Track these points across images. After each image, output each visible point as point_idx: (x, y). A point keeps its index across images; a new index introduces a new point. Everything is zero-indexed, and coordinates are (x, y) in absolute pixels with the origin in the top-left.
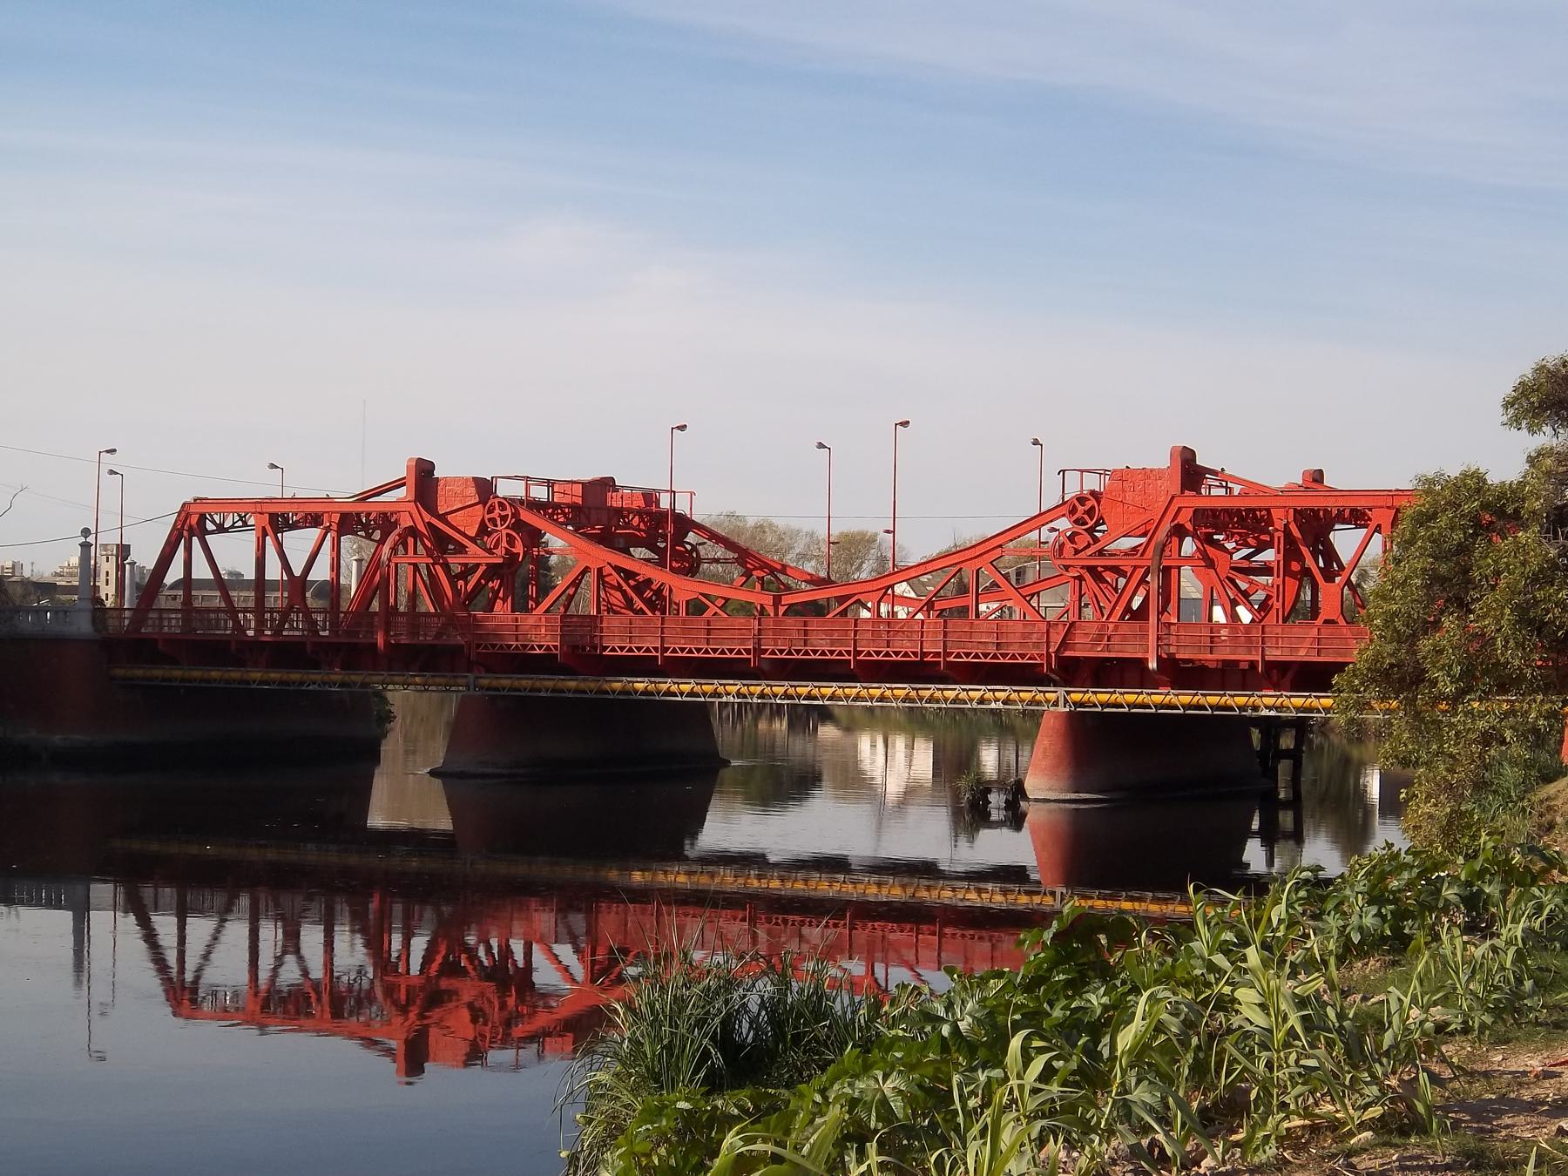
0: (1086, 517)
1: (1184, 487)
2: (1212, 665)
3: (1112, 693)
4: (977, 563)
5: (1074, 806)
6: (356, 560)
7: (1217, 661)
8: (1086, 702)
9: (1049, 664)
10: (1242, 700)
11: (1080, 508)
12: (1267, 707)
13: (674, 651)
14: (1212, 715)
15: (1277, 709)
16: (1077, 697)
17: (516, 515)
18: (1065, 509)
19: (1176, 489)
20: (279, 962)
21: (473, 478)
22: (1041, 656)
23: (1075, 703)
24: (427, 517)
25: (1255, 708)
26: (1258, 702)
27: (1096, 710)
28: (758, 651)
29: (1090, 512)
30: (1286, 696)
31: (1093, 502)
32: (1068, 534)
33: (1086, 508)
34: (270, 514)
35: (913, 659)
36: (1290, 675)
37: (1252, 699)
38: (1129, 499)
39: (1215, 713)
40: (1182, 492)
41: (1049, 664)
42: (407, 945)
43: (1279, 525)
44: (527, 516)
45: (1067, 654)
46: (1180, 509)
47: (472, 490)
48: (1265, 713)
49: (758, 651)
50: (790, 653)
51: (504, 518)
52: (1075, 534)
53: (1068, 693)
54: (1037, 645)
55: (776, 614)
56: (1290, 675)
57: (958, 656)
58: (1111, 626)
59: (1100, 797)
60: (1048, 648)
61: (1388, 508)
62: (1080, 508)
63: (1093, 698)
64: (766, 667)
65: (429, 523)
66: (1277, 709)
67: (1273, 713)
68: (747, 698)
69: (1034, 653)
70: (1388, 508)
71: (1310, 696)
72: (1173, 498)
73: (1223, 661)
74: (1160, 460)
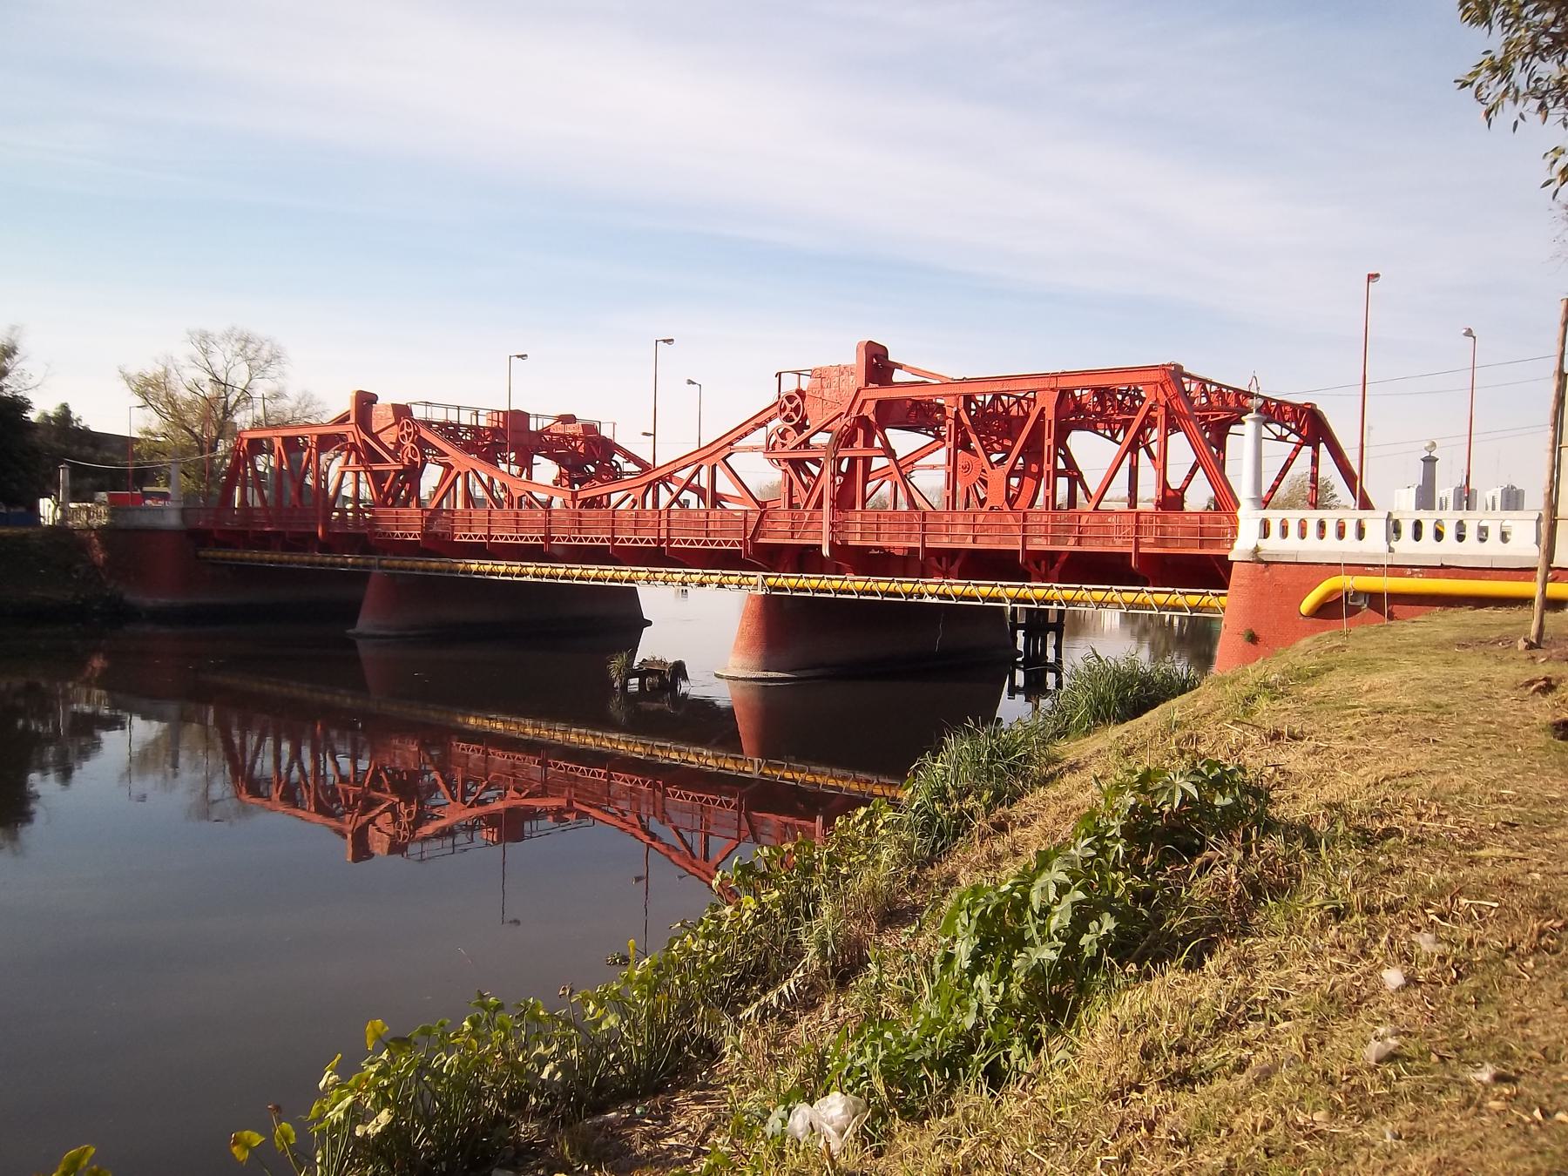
0: (793, 414)
1: (869, 379)
2: (897, 552)
3: (1139, 592)
4: (712, 461)
5: (761, 684)
6: (1252, 419)
7: (904, 548)
8: (1203, 607)
9: (746, 550)
10: (908, 587)
11: (789, 406)
12: (930, 595)
13: (622, 541)
14: (858, 600)
15: (941, 596)
16: (771, 581)
17: (417, 432)
18: (776, 410)
19: (861, 382)
20: (290, 769)
21: (393, 405)
22: (740, 542)
23: (770, 587)
24: (363, 436)
25: (921, 596)
26: (923, 589)
27: (877, 598)
28: (547, 538)
29: (796, 410)
30: (1029, 587)
31: (799, 400)
32: (780, 431)
33: (793, 405)
34: (283, 437)
35: (653, 545)
36: (957, 563)
37: (917, 586)
38: (826, 396)
39: (1194, 614)
40: (867, 385)
41: (746, 550)
42: (243, 740)
43: (950, 413)
44: (425, 434)
45: (761, 540)
46: (864, 401)
47: (390, 414)
48: (928, 600)
49: (547, 538)
50: (569, 540)
51: (409, 434)
52: (786, 430)
53: (765, 577)
54: (737, 532)
55: (574, 507)
56: (957, 563)
57: (678, 542)
58: (807, 514)
59: (787, 675)
60: (745, 536)
61: (1052, 389)
62: (789, 406)
63: (1149, 599)
64: (558, 552)
65: (364, 441)
66: (941, 596)
67: (936, 600)
68: (1062, 605)
69: (731, 540)
70: (1052, 389)
71: (1023, 586)
72: (859, 391)
73: (909, 548)
74: (850, 357)
